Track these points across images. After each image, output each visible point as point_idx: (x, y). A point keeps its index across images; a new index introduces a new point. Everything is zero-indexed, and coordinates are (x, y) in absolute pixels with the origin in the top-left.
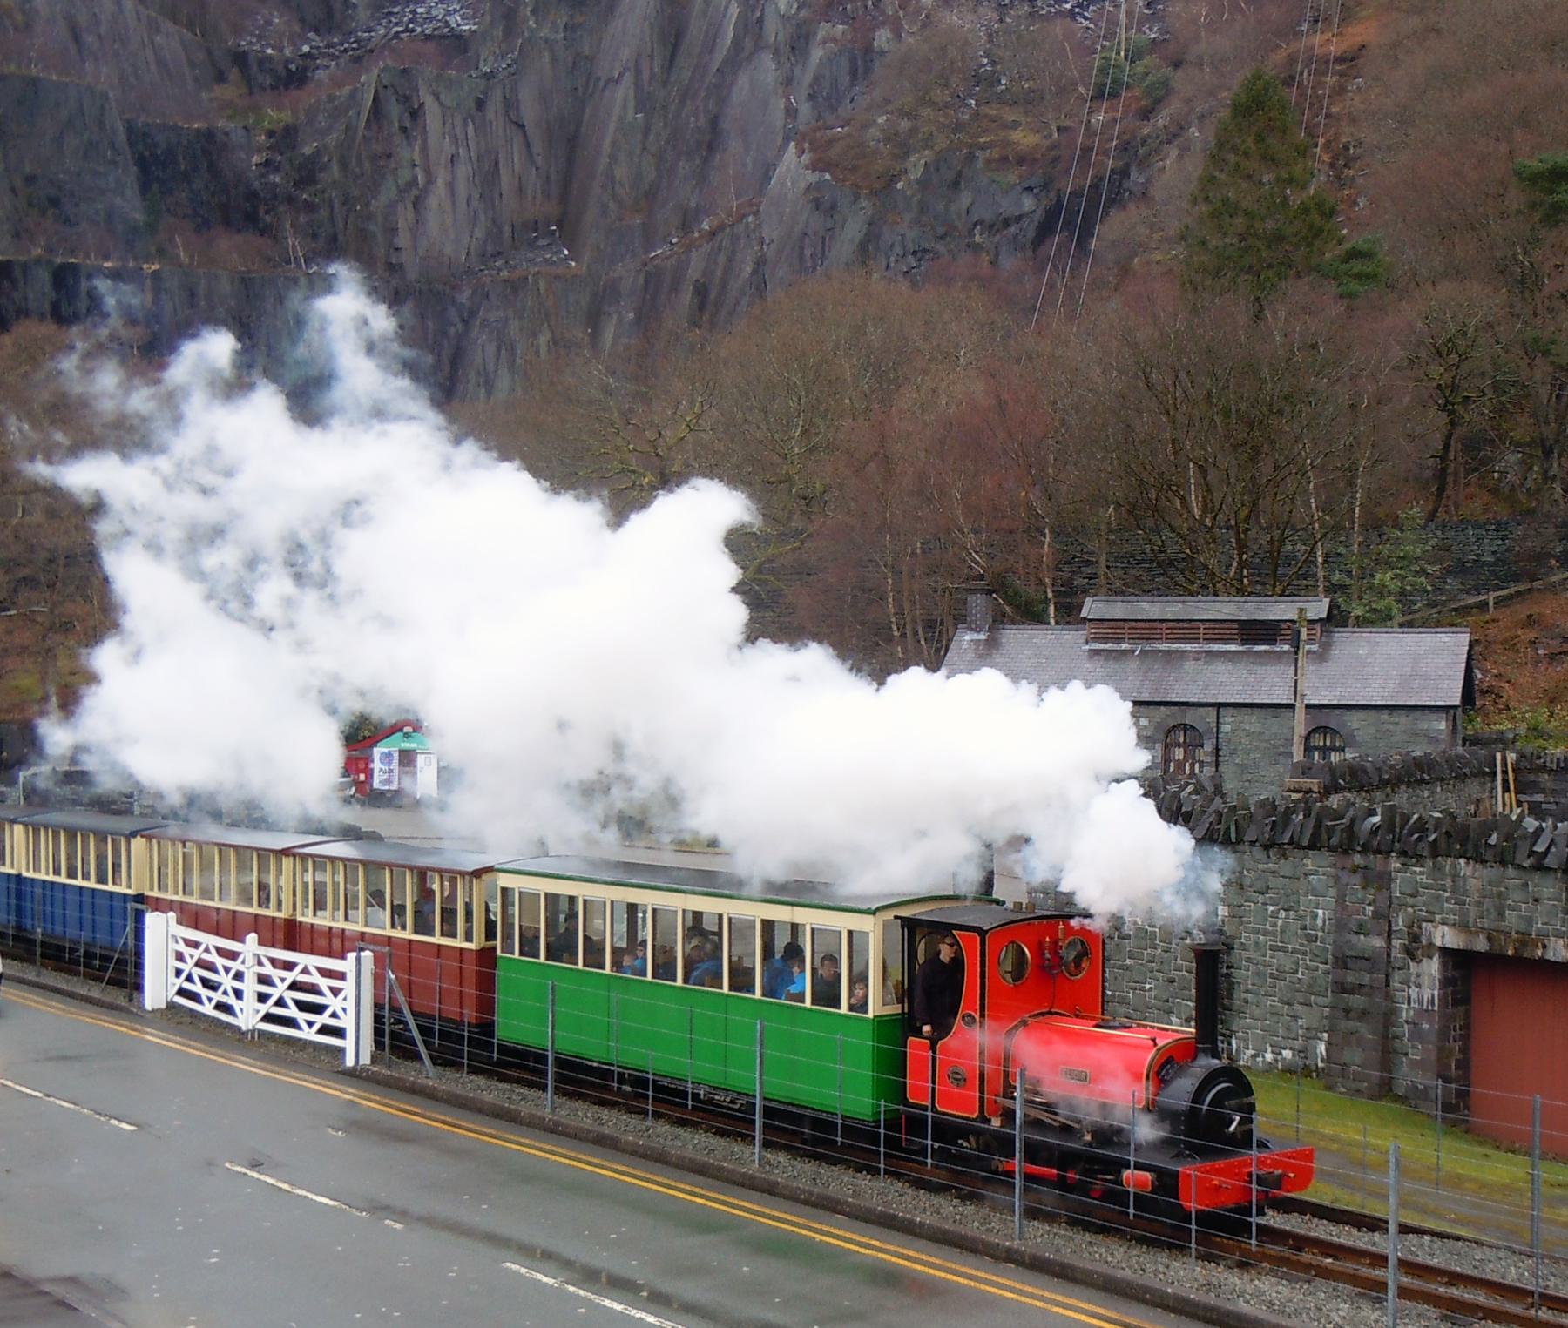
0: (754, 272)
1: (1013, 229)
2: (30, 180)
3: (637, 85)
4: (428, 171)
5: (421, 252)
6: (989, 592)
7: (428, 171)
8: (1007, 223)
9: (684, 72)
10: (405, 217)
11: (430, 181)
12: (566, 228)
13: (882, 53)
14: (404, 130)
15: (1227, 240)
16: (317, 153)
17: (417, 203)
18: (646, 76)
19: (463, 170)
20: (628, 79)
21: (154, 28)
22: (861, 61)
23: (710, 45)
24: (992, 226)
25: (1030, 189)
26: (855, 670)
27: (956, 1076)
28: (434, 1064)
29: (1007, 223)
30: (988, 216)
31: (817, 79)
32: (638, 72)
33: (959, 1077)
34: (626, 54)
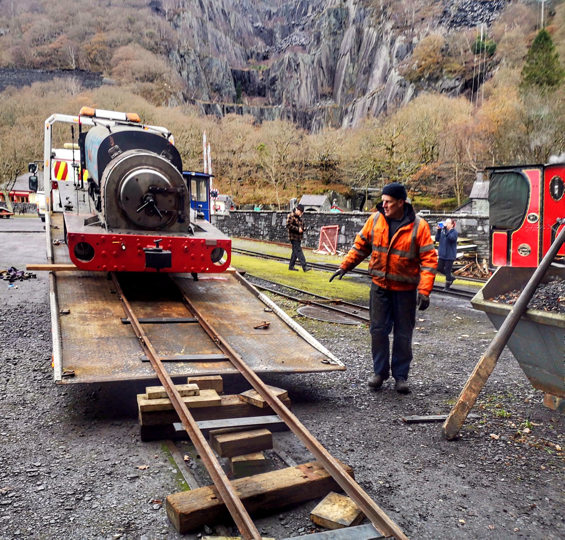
0: (384, 104)
1: (453, 90)
2: (212, 84)
3: (351, 55)
4: (301, 81)
5: (300, 101)
6: (483, 172)
7: (301, 81)
8: (452, 89)
9: (362, 53)
10: (296, 93)
11: (301, 83)
12: (332, 95)
13: (415, 44)
14: (295, 70)
15: (65, 303)
16: (275, 76)
17: (299, 89)
18: (353, 53)
19: (309, 80)
20: (348, 54)
21: (234, 45)
22: (410, 47)
23: (369, 43)
24: (447, 90)
25: (458, 79)
26: (357, 258)
27: (523, 250)
28: (196, 421)
29: (452, 89)
30: (447, 87)
31: (398, 52)
32: (351, 52)
33: (526, 250)
34: (348, 47)
